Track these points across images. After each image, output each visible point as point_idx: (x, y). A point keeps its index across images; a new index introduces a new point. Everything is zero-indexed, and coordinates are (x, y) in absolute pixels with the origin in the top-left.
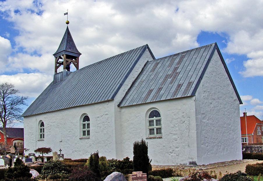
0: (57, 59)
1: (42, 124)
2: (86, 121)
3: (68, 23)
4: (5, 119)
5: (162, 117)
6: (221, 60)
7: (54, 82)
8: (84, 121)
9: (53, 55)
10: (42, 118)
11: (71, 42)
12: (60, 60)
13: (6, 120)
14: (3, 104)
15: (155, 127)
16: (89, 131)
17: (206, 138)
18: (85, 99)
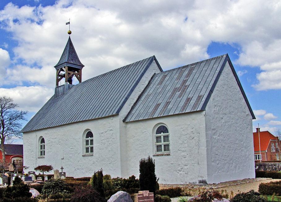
1: (90, 134)
2: (89, 137)
3: (70, 33)
5: (170, 133)
8: (87, 137)
9: (55, 67)
12: (62, 73)
15: (162, 143)
16: (92, 148)
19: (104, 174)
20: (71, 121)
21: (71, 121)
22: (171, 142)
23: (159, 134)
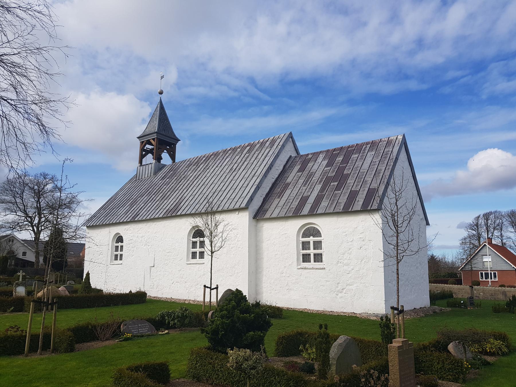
0: (144, 144)
1: (120, 239)
2: (120, 243)
3: (161, 93)
4: (38, 228)
5: (324, 238)
6: (408, 161)
7: (138, 178)
8: (117, 242)
9: (138, 138)
10: (121, 230)
11: (165, 122)
12: (148, 147)
13: (40, 230)
14: (37, 206)
15: (312, 251)
16: (121, 255)
17: (394, 273)
18: (162, 210)
19: (246, 297)
20: (145, 217)
21: (145, 217)
22: (324, 251)
23: (306, 237)
